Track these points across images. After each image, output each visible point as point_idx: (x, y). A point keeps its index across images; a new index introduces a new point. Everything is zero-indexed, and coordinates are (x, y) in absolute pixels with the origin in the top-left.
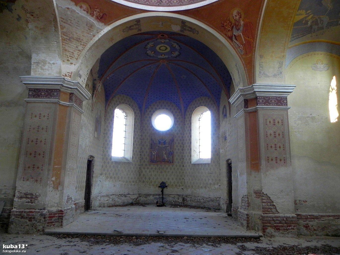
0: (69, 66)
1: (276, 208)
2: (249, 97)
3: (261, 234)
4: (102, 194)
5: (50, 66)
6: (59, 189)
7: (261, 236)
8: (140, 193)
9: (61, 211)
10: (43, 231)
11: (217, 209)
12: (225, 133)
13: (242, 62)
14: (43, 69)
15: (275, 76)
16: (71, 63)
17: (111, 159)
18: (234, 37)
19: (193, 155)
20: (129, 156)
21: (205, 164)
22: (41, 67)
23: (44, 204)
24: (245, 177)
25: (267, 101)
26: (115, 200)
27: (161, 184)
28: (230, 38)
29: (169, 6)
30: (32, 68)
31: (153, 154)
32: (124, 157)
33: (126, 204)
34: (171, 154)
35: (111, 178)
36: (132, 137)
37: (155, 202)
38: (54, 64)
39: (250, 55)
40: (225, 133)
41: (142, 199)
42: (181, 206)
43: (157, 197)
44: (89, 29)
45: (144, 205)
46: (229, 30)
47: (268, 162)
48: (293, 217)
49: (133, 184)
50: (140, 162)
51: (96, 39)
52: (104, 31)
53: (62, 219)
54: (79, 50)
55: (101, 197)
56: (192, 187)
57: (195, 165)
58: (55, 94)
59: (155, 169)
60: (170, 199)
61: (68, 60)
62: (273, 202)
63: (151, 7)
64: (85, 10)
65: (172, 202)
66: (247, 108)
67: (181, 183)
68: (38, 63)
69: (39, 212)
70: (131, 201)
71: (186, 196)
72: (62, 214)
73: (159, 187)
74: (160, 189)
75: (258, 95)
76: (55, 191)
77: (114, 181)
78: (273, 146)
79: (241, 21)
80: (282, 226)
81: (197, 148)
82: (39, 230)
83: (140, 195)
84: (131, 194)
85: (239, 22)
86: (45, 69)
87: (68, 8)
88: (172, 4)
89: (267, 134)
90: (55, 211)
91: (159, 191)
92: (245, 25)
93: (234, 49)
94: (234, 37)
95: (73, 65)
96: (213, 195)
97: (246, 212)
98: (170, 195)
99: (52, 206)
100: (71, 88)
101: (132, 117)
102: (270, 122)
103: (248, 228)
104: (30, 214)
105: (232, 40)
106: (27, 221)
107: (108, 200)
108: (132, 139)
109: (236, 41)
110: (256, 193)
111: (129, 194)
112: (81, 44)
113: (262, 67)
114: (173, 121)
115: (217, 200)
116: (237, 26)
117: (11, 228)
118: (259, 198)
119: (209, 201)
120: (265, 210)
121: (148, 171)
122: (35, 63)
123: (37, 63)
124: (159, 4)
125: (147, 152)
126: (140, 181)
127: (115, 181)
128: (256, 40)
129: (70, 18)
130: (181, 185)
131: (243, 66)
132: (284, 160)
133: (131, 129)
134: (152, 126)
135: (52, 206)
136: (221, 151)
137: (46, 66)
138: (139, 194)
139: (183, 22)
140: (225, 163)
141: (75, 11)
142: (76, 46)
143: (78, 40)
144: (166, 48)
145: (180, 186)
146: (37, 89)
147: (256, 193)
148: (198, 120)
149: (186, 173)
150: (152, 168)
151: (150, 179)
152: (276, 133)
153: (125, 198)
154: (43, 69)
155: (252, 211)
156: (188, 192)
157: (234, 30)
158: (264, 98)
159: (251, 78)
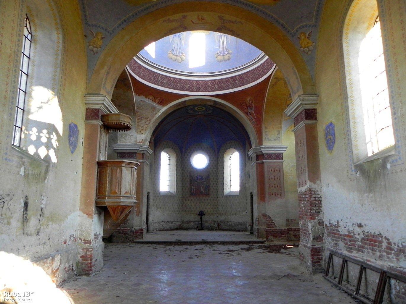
0: (141, 135)
1: (274, 224)
2: (259, 154)
3: (265, 240)
4: (154, 221)
5: (130, 137)
6: (139, 216)
7: (265, 241)
8: (183, 220)
9: (142, 229)
10: (133, 241)
11: (245, 230)
12: (249, 171)
13: (255, 129)
14: (126, 139)
15: (275, 140)
16: (142, 134)
17: (160, 193)
18: (249, 113)
20: (173, 190)
21: (235, 196)
22: (124, 138)
23: (132, 225)
24: (257, 205)
25: (270, 156)
26: (164, 226)
27: (200, 212)
28: (247, 113)
29: (206, 91)
30: (118, 138)
31: (193, 188)
32: (169, 191)
33: (172, 229)
34: (208, 187)
35: (160, 208)
36: (175, 175)
37: (196, 227)
38: (132, 135)
39: (259, 126)
40: (249, 171)
41: (185, 225)
42: (216, 230)
43: (197, 223)
44: (153, 110)
45: (187, 229)
46: (245, 109)
47: (270, 196)
48: (285, 229)
49: (177, 213)
50: (182, 195)
51: (157, 116)
52: (162, 110)
53: (142, 234)
54: (147, 124)
55: (154, 224)
56: (225, 214)
57: (227, 196)
60: (207, 224)
61: (140, 132)
62: (273, 220)
63: (193, 92)
64: (151, 100)
65: (209, 226)
66: (258, 160)
67: (216, 211)
69: (130, 230)
70: (176, 227)
71: (221, 222)
72: (143, 231)
73: (198, 215)
74: (199, 217)
75: (264, 153)
77: (163, 211)
78: (274, 186)
79: (253, 104)
81: (229, 182)
82: (130, 241)
83: (183, 222)
84: (176, 221)
85: (252, 104)
86: (127, 139)
87: (141, 101)
88: (207, 90)
90: (138, 229)
92: (256, 107)
93: (250, 121)
94: (249, 113)
95: (143, 135)
96: (241, 220)
97: (257, 228)
99: (136, 226)
100: (143, 151)
101: (174, 158)
102: (272, 170)
103: (258, 237)
104: (125, 231)
105: (248, 115)
106: (123, 235)
107: (158, 226)
108: (175, 176)
109: (250, 116)
110: (263, 215)
111: (174, 221)
113: (267, 134)
114: (208, 159)
115: (244, 224)
116: (251, 106)
117: (114, 239)
118: (265, 218)
119: (238, 225)
120: (268, 225)
121: (189, 202)
122: (120, 135)
123: (121, 135)
124: (198, 91)
125: (187, 187)
126: (183, 211)
127: (164, 211)
128: (263, 117)
129: (142, 106)
130: (216, 213)
131: (255, 133)
132: (280, 194)
133: (174, 168)
134: (191, 165)
135: (136, 226)
136: (247, 185)
137: (127, 137)
138: (182, 221)
139: (215, 102)
140: (249, 194)
141: (145, 101)
142: (145, 122)
143: (146, 118)
145: (215, 214)
147: (263, 215)
148: (229, 159)
149: (220, 203)
150: (192, 200)
151: (190, 208)
152: (275, 177)
153: (171, 224)
154: (126, 139)
155: (260, 227)
156: (222, 218)
157: (249, 108)
158: (268, 154)
159: (261, 143)
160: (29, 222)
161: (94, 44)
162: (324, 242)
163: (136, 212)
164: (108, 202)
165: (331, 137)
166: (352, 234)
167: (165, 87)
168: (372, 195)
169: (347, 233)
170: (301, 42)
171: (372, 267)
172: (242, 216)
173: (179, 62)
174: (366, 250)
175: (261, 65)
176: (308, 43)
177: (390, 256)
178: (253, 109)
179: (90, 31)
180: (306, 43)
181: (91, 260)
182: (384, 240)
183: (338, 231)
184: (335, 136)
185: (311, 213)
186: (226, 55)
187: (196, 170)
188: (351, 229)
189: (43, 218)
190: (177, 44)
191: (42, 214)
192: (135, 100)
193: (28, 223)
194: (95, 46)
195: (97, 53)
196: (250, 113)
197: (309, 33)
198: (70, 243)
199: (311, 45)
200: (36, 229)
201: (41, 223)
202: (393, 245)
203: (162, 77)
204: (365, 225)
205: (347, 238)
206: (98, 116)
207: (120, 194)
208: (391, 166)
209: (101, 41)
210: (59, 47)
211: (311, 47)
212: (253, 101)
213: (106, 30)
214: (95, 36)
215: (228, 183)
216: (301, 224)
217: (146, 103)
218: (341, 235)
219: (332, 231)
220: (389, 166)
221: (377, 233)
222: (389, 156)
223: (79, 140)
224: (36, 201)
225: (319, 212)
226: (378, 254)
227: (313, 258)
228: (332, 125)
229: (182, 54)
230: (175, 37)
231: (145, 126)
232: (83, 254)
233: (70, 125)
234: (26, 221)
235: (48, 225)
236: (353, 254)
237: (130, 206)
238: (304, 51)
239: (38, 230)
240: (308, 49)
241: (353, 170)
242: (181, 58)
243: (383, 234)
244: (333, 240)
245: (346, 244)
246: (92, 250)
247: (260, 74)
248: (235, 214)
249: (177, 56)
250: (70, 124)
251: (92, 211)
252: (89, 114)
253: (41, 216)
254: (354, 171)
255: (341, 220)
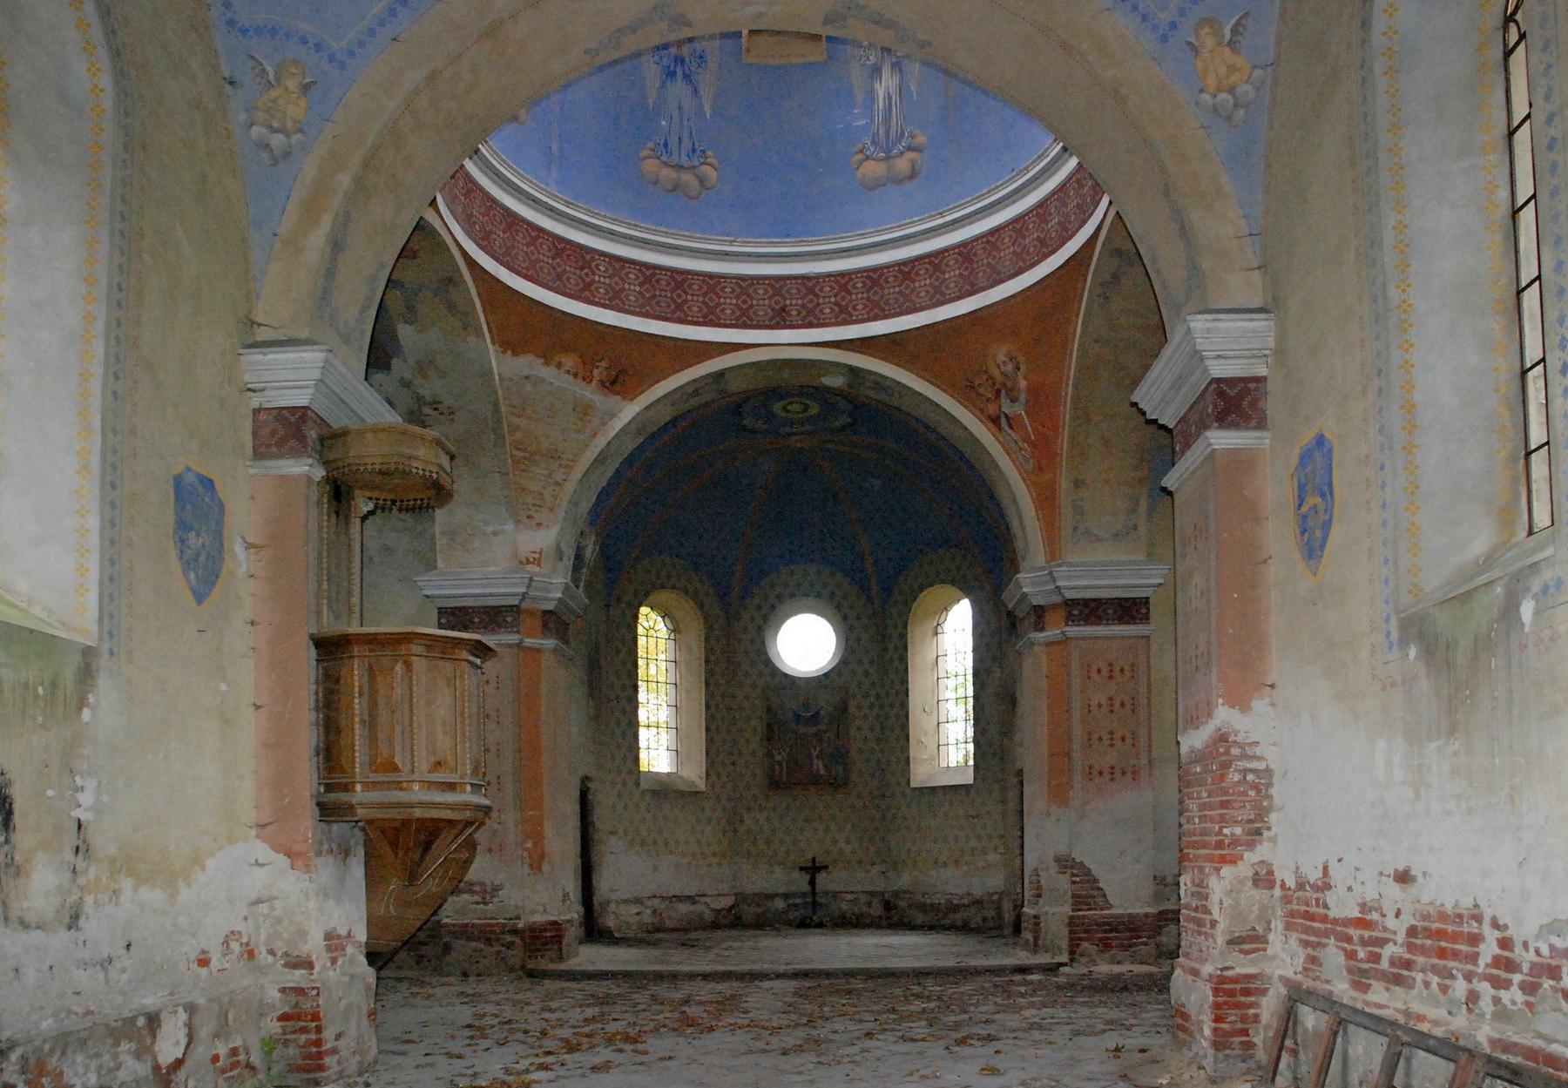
1: (1105, 896)
3: (1064, 958)
7: (1064, 965)
16: (539, 525)
18: (1003, 421)
19: (915, 758)
28: (995, 421)
29: (810, 325)
34: (840, 756)
35: (643, 843)
39: (1048, 476)
44: (581, 420)
48: (1146, 915)
49: (714, 860)
51: (601, 442)
54: (557, 484)
58: (509, 619)
59: (788, 808)
68: (452, 534)
70: (709, 916)
76: (535, 874)
78: (1106, 737)
80: (1117, 938)
84: (709, 893)
89: (1089, 706)
91: (801, 882)
94: (1003, 421)
98: (840, 892)
99: (533, 912)
102: (1099, 671)
105: (1000, 429)
107: (638, 914)
109: (1010, 431)
110: (1058, 860)
112: (560, 465)
121: (762, 817)
139: (854, 371)
144: (807, 408)
146: (460, 609)
156: (904, 880)
160: (28, 877)
161: (272, 117)
162: (1270, 952)
163: (530, 857)
164: (363, 805)
165: (1319, 500)
166: (1375, 916)
167: (627, 312)
168: (1456, 745)
169: (1356, 914)
170: (1200, 64)
171: (1431, 1042)
172: (984, 868)
173: (691, 198)
174: (1419, 977)
175: (1054, 193)
176: (1232, 68)
177: (1502, 993)
178: (1023, 397)
179: (252, 57)
180: (1223, 71)
181: (319, 1030)
182: (1487, 930)
183: (1326, 906)
184: (1332, 494)
185: (1226, 835)
186: (902, 153)
187: (790, 683)
188: (1371, 895)
189: (89, 864)
190: (681, 115)
191: (83, 848)
192: (500, 375)
193: (22, 880)
194: (275, 124)
195: (287, 154)
196: (1006, 415)
197: (1238, 23)
198: (227, 966)
199: (1246, 82)
200: (63, 906)
201: (82, 881)
202: (1518, 949)
203: (644, 274)
204: (1425, 874)
205: (1355, 933)
206: (302, 439)
207: (413, 771)
208: (1537, 613)
209: (303, 103)
210: (102, 130)
211: (1247, 87)
212: (1023, 368)
213: (318, 47)
214: (271, 77)
215: (926, 735)
216: (1186, 885)
217: (549, 388)
218: (1335, 921)
219: (1304, 908)
220: (1527, 609)
221: (1466, 903)
222: (1534, 567)
223: (226, 544)
224: (50, 793)
225: (1258, 832)
226: (1460, 988)
227: (1218, 1019)
228: (1323, 444)
229: (702, 160)
230: (669, 83)
231: (547, 493)
232: (287, 1009)
233: (178, 480)
234: (12, 870)
235: (114, 891)
236: (1371, 997)
237: (458, 822)
238: (1214, 105)
239: (71, 908)
240: (1230, 98)
241: (1395, 642)
242: (697, 176)
243: (1483, 904)
244: (1306, 944)
245: (1351, 955)
246: (318, 995)
247: (1051, 239)
248: (956, 861)
249: (680, 167)
250: (180, 475)
251: (306, 841)
252: (265, 432)
253: (81, 855)
254: (1395, 648)
255: (1340, 860)
